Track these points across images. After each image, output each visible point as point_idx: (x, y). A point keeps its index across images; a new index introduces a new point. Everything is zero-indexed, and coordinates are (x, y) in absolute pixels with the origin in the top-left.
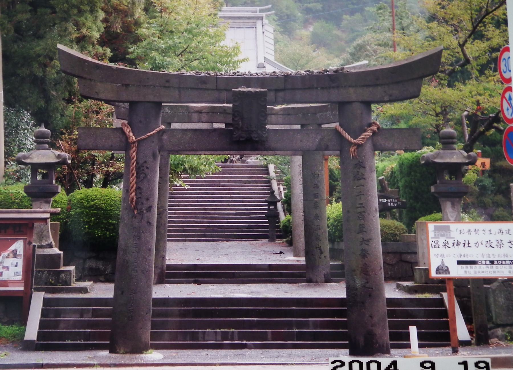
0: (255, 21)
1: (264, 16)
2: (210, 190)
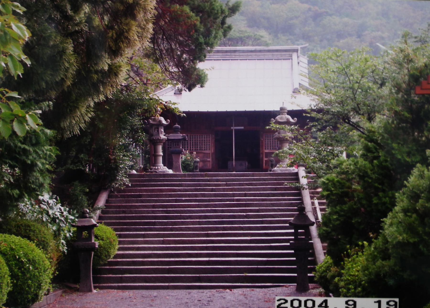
0: (291, 53)
1: (299, 48)
2: (220, 206)
